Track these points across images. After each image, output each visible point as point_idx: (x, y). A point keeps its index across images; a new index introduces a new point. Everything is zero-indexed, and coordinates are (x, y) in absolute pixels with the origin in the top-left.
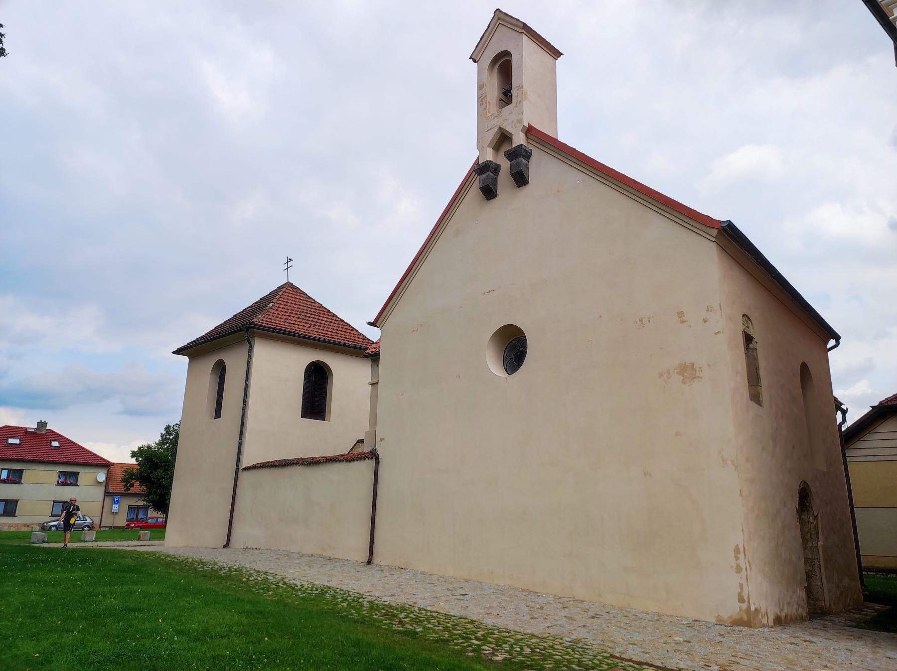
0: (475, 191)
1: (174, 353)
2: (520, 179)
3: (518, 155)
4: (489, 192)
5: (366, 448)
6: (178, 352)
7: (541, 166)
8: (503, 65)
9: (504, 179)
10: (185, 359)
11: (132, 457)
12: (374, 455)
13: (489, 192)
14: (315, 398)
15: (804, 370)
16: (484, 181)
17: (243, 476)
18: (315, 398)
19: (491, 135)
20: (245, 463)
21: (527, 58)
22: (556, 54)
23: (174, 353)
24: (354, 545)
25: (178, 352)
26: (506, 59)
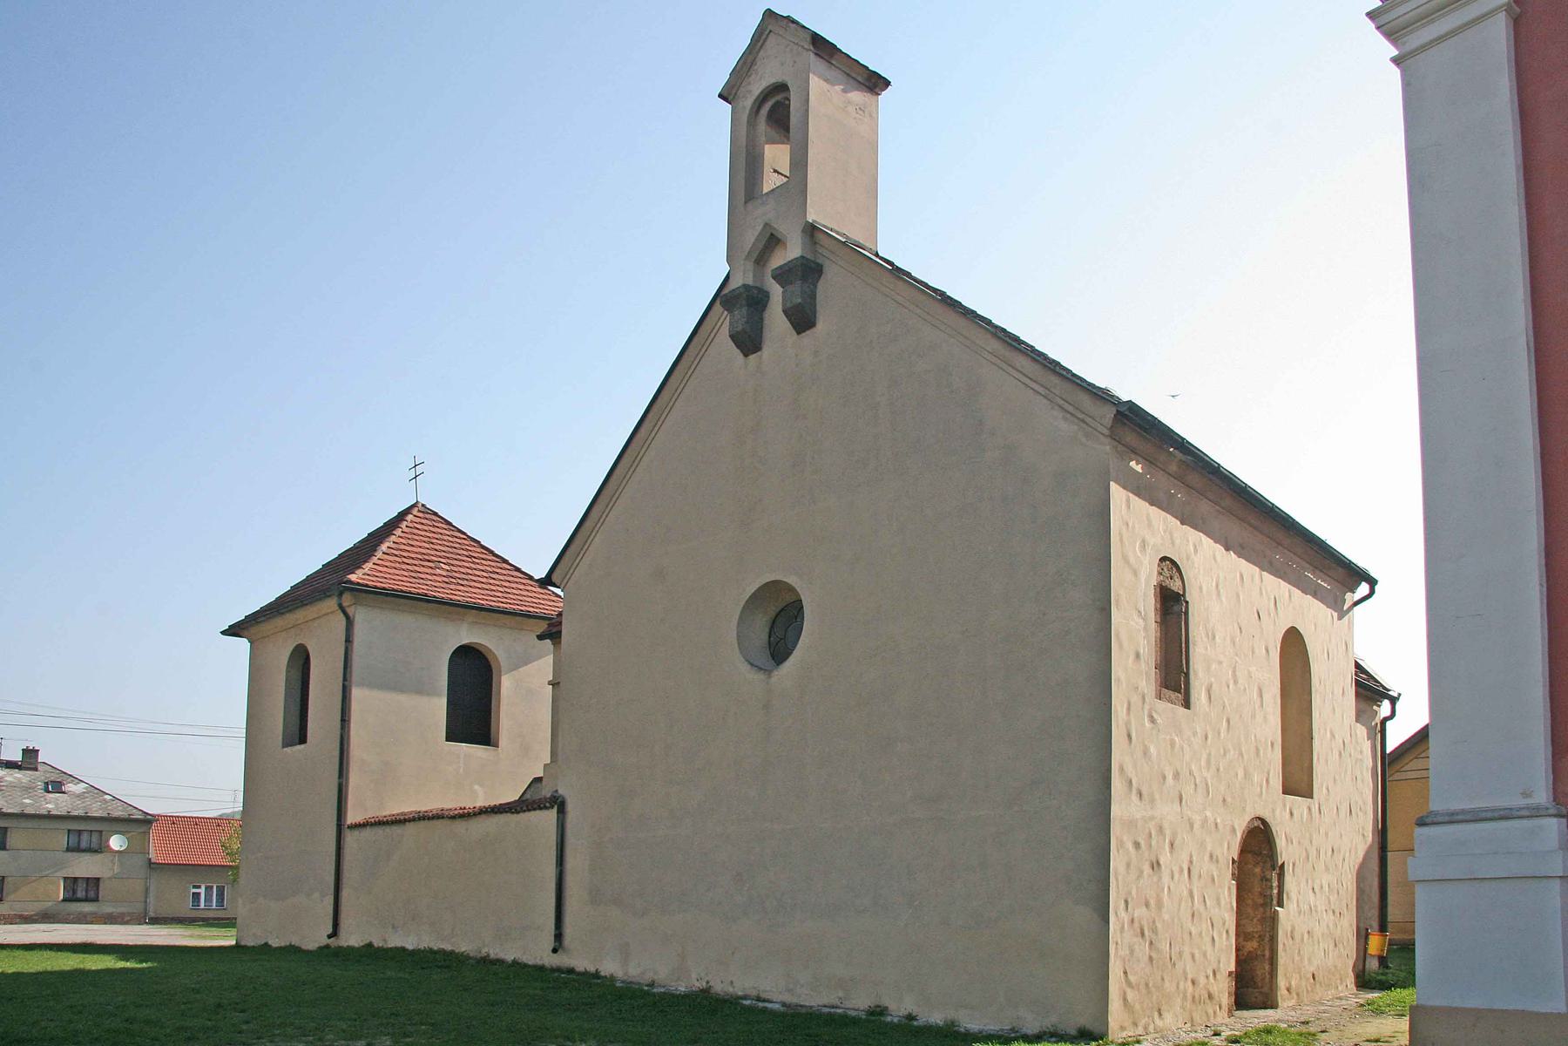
0: (723, 344)
1: (223, 633)
2: (802, 320)
3: (807, 272)
4: (749, 342)
5: (546, 792)
6: (234, 631)
7: (833, 291)
8: (812, 236)
9: (776, 320)
10: (242, 645)
11: (26, 752)
12: (558, 803)
13: (749, 342)
14: (472, 717)
15: (1293, 644)
16: (738, 312)
17: (350, 838)
18: (472, 717)
19: (750, 237)
20: (352, 817)
21: (823, 96)
22: (875, 83)
23: (223, 633)
24: (549, 942)
25: (234, 631)
26: (782, 90)
